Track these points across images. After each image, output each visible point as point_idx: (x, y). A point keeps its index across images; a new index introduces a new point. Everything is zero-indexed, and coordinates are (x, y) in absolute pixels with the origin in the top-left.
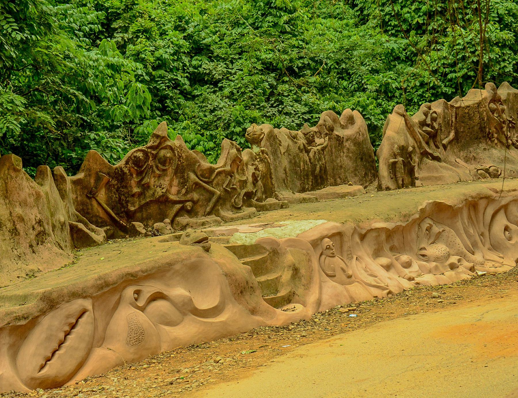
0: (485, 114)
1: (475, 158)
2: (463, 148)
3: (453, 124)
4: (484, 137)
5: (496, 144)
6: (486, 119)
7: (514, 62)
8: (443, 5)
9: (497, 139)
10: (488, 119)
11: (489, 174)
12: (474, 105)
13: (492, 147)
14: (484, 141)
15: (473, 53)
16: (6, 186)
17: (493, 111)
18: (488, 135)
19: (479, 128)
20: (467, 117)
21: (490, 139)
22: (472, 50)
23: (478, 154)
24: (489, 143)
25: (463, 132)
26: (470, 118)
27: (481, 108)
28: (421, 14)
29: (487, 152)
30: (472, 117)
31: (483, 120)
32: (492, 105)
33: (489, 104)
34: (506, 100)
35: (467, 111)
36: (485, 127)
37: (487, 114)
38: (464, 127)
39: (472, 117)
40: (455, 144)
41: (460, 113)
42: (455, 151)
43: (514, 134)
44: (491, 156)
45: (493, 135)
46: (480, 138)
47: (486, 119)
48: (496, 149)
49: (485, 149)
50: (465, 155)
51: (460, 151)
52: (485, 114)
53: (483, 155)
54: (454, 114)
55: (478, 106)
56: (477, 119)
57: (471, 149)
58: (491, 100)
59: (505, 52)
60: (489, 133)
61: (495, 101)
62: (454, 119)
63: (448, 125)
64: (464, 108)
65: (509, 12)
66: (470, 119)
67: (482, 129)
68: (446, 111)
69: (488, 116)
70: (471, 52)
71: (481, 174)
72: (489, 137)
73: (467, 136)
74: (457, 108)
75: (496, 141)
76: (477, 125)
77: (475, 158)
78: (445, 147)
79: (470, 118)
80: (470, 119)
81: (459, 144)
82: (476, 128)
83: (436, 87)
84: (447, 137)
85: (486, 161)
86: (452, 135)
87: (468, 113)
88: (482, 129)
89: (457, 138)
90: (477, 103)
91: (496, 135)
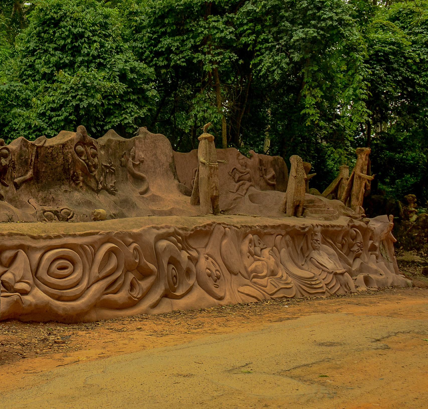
0: (69, 155)
1: (53, 200)
2: (42, 189)
3: (33, 163)
4: (67, 179)
5: (81, 187)
6: (70, 161)
7: (136, 115)
8: (72, 58)
9: (83, 182)
10: (73, 161)
11: (58, 216)
12: (58, 145)
13: (76, 190)
14: (67, 183)
15: (74, 97)
16: (70, 235)
17: (80, 154)
18: (72, 177)
19: (63, 170)
20: (50, 158)
21: (74, 181)
22: (74, 94)
23: (57, 195)
24: (73, 185)
25: (44, 172)
26: (53, 158)
27: (66, 149)
28: (51, 65)
29: (67, 195)
30: (55, 158)
31: (68, 161)
32: (80, 148)
33: (76, 145)
34: (105, 145)
35: (50, 151)
36: (69, 169)
37: (72, 156)
38: (46, 167)
39: (55, 158)
40: (34, 184)
41: (43, 152)
42: (33, 191)
43: (112, 180)
44: (69, 198)
45: (78, 178)
46: (63, 180)
47: (70, 161)
48: (79, 192)
49: (66, 191)
50: (44, 196)
51: (39, 191)
52: (69, 155)
53: (62, 197)
54: (34, 153)
55: (63, 147)
56: (60, 160)
57: (52, 190)
58: (79, 142)
59: (128, 106)
60: (74, 175)
61: (84, 144)
62: (33, 158)
63: (25, 163)
64: (46, 147)
65: (133, 70)
66: (53, 159)
67: (66, 171)
68: (24, 149)
69: (73, 158)
70: (72, 96)
71: (47, 216)
72: (74, 179)
73: (49, 176)
74: (38, 147)
75: (81, 184)
76: (60, 167)
77: (53, 200)
78: (17, 186)
79: (53, 158)
80: (53, 159)
81: (40, 185)
82: (59, 169)
83: (41, 129)
84: (22, 176)
85: (63, 203)
86: (30, 174)
87: (51, 153)
88: (66, 171)
89: (37, 177)
90: (62, 144)
91: (81, 178)
